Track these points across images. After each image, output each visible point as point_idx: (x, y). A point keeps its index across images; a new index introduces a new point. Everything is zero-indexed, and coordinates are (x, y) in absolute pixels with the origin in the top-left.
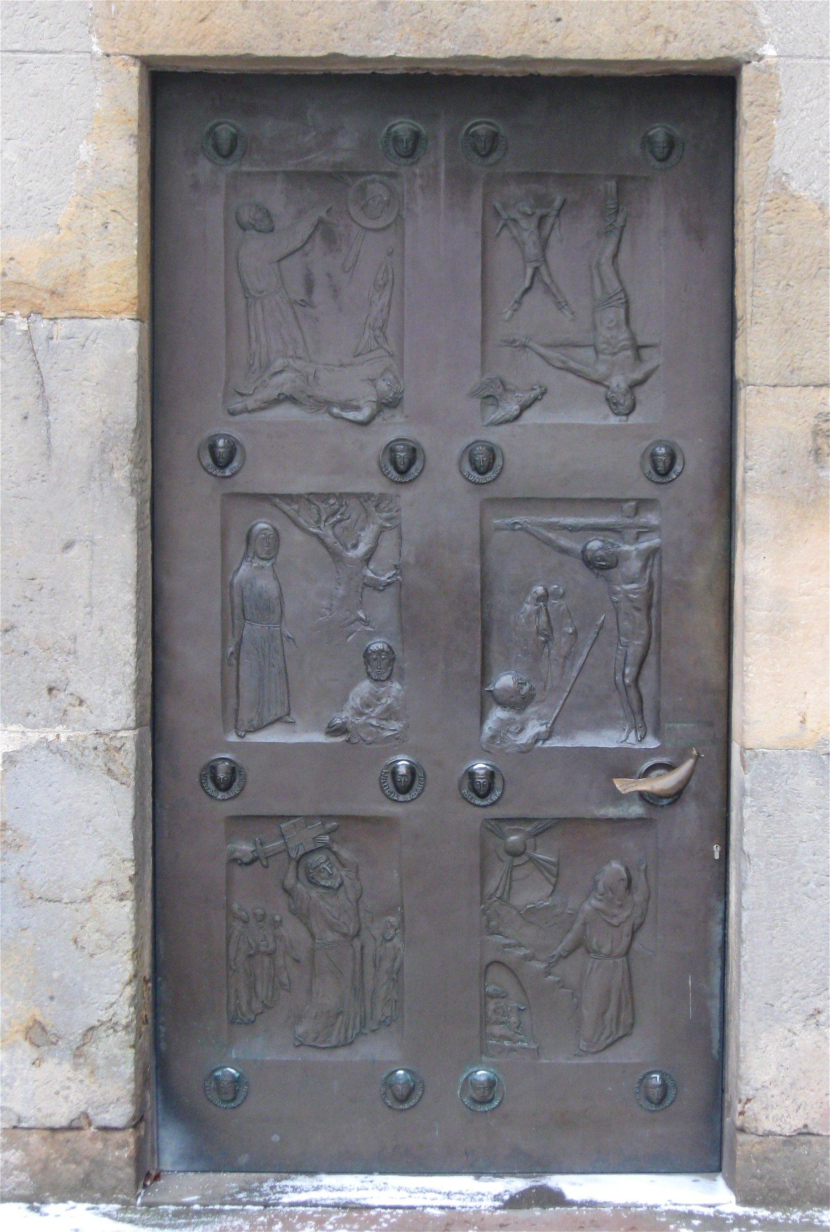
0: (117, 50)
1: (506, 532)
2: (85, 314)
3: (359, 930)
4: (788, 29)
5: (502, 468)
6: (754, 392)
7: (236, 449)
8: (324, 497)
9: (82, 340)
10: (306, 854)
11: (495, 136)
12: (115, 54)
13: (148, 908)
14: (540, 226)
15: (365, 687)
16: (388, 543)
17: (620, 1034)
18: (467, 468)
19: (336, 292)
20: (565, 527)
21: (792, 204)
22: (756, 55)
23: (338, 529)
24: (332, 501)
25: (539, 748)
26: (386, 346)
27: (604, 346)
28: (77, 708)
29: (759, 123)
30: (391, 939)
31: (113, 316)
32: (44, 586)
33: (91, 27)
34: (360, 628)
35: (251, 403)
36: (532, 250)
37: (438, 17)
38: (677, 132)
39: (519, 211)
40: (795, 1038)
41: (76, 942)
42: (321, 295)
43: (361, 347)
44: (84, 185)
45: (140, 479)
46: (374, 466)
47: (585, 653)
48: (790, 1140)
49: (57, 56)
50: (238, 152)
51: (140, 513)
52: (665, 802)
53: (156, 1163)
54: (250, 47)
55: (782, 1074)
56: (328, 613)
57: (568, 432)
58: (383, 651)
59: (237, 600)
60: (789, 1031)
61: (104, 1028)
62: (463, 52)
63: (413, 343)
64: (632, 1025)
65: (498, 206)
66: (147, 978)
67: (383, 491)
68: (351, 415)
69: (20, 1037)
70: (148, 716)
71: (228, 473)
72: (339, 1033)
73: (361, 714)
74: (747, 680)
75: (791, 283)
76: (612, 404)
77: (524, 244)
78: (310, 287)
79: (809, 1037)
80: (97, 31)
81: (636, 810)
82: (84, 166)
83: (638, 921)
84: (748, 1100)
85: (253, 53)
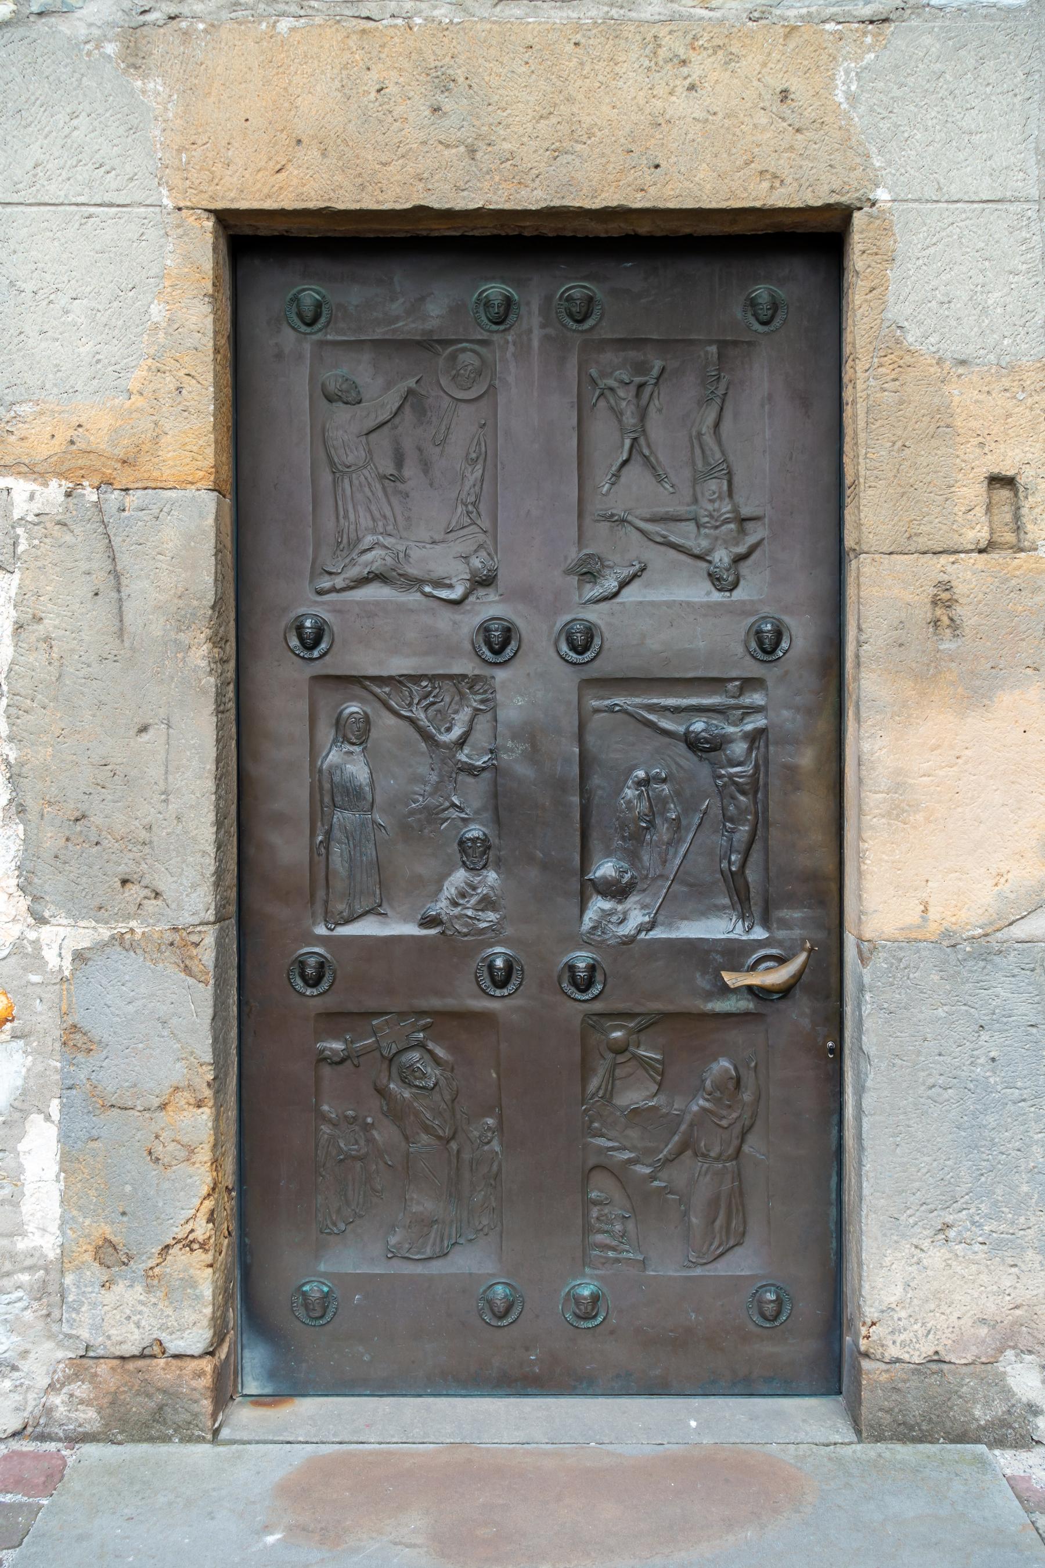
0: (189, 204)
1: (604, 714)
2: (159, 485)
3: (455, 1133)
4: (903, 171)
5: (601, 647)
6: (869, 561)
7: (324, 630)
8: (416, 679)
9: (156, 511)
10: (399, 1052)
11: (590, 300)
12: (187, 208)
13: (232, 1114)
14: (638, 395)
15: (460, 876)
16: (483, 724)
17: (731, 1243)
18: (564, 648)
19: (426, 466)
20: (666, 708)
21: (908, 358)
22: (869, 199)
23: (431, 711)
24: (424, 684)
25: (643, 940)
26: (479, 522)
27: (707, 519)
28: (154, 902)
29: (872, 273)
30: (488, 1143)
31: (189, 486)
32: (117, 772)
33: (161, 179)
34: (454, 814)
35: (339, 582)
36: (630, 419)
37: (529, 165)
38: (781, 293)
39: (616, 380)
40: (923, 1255)
41: (150, 1153)
42: (410, 471)
43: (453, 524)
44: (156, 348)
45: (221, 659)
46: (468, 646)
47: (689, 840)
48: (918, 1370)
49: (124, 209)
50: (323, 320)
51: (220, 694)
52: (776, 996)
53: (240, 1386)
54: (330, 199)
55: (909, 1296)
56: (421, 799)
57: (671, 608)
58: (478, 838)
59: (327, 786)
60: (916, 1247)
61: (180, 1246)
62: (557, 203)
63: (515, 544)
64: (744, 1234)
65: (595, 374)
66: (230, 1187)
67: (477, 672)
68: (444, 594)
69: (88, 1257)
70: (232, 909)
71: (316, 654)
72: (434, 1244)
73: (455, 904)
74: (864, 867)
75: (907, 444)
76: (715, 579)
77: (622, 414)
78: (399, 460)
79: (938, 1254)
80: (167, 183)
81: (745, 1004)
82: (156, 327)
83: (747, 1123)
84: (873, 1324)
85: (333, 205)
